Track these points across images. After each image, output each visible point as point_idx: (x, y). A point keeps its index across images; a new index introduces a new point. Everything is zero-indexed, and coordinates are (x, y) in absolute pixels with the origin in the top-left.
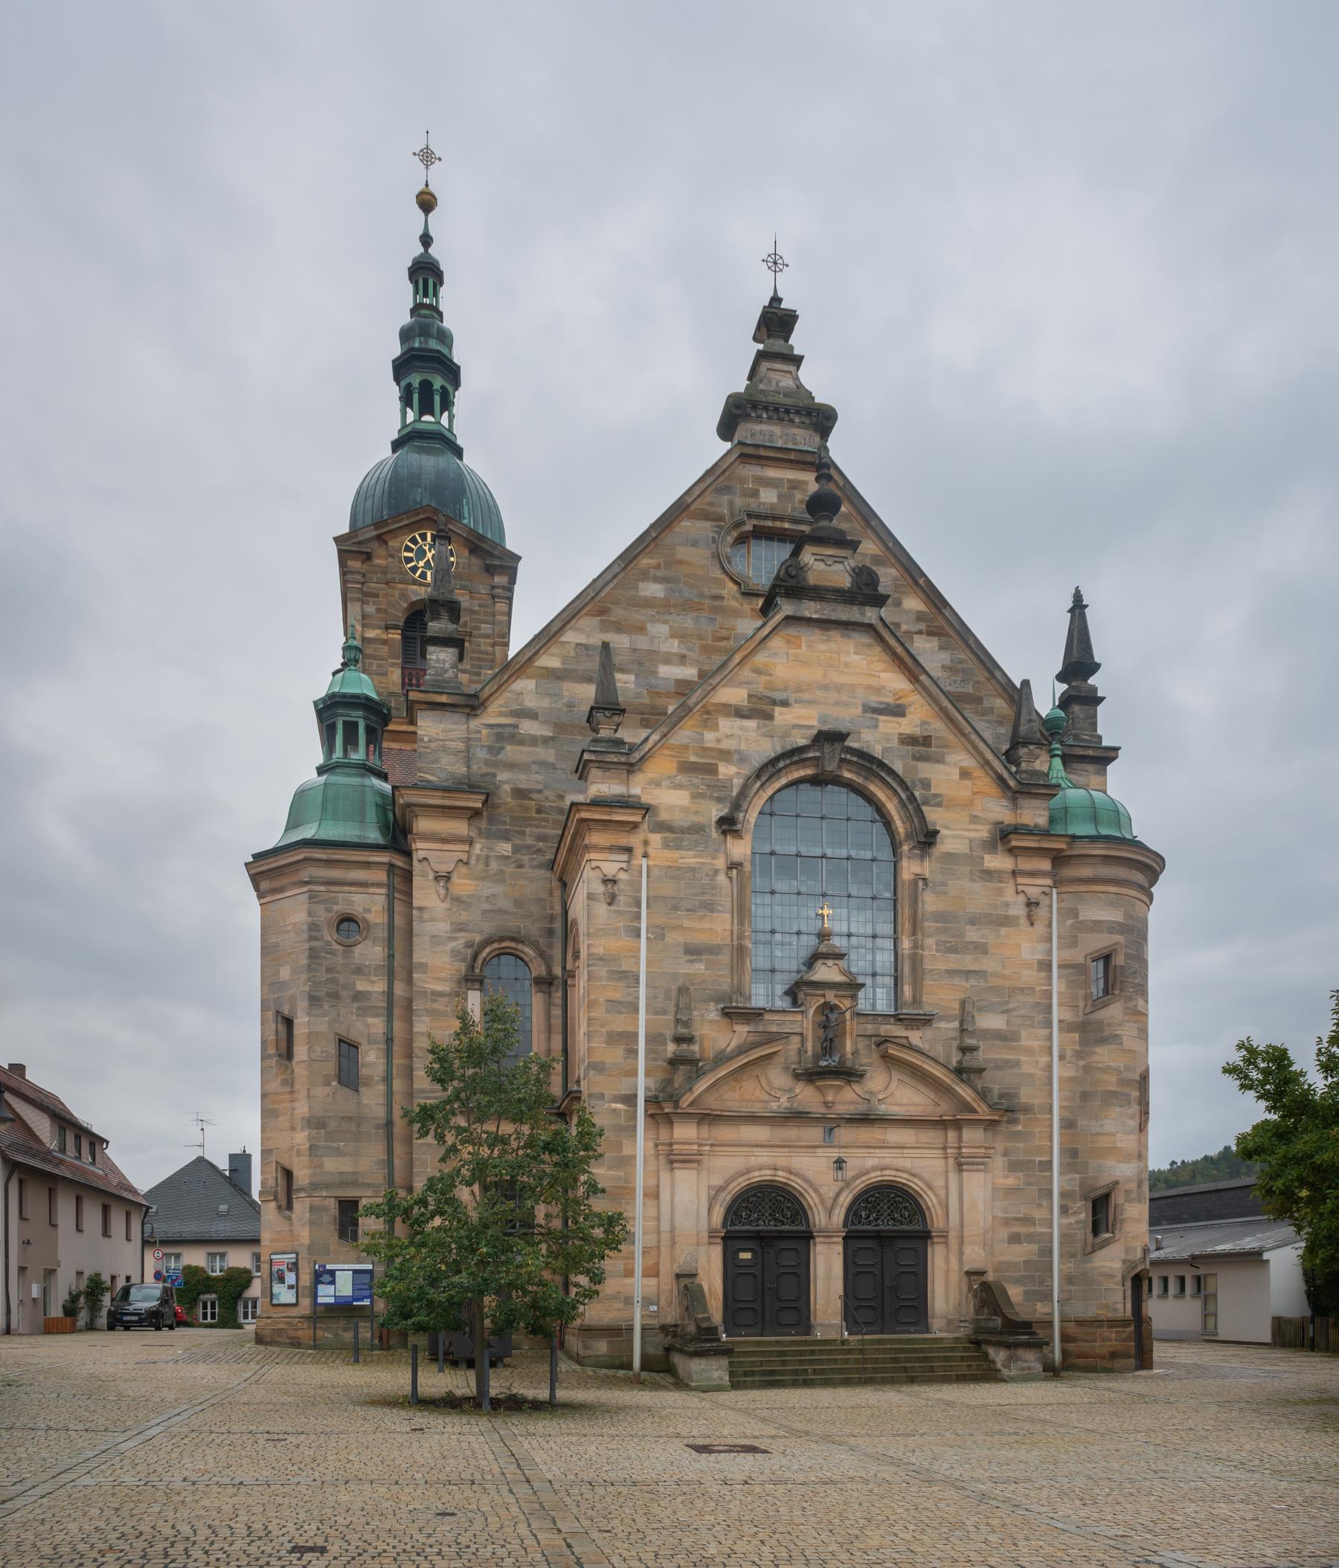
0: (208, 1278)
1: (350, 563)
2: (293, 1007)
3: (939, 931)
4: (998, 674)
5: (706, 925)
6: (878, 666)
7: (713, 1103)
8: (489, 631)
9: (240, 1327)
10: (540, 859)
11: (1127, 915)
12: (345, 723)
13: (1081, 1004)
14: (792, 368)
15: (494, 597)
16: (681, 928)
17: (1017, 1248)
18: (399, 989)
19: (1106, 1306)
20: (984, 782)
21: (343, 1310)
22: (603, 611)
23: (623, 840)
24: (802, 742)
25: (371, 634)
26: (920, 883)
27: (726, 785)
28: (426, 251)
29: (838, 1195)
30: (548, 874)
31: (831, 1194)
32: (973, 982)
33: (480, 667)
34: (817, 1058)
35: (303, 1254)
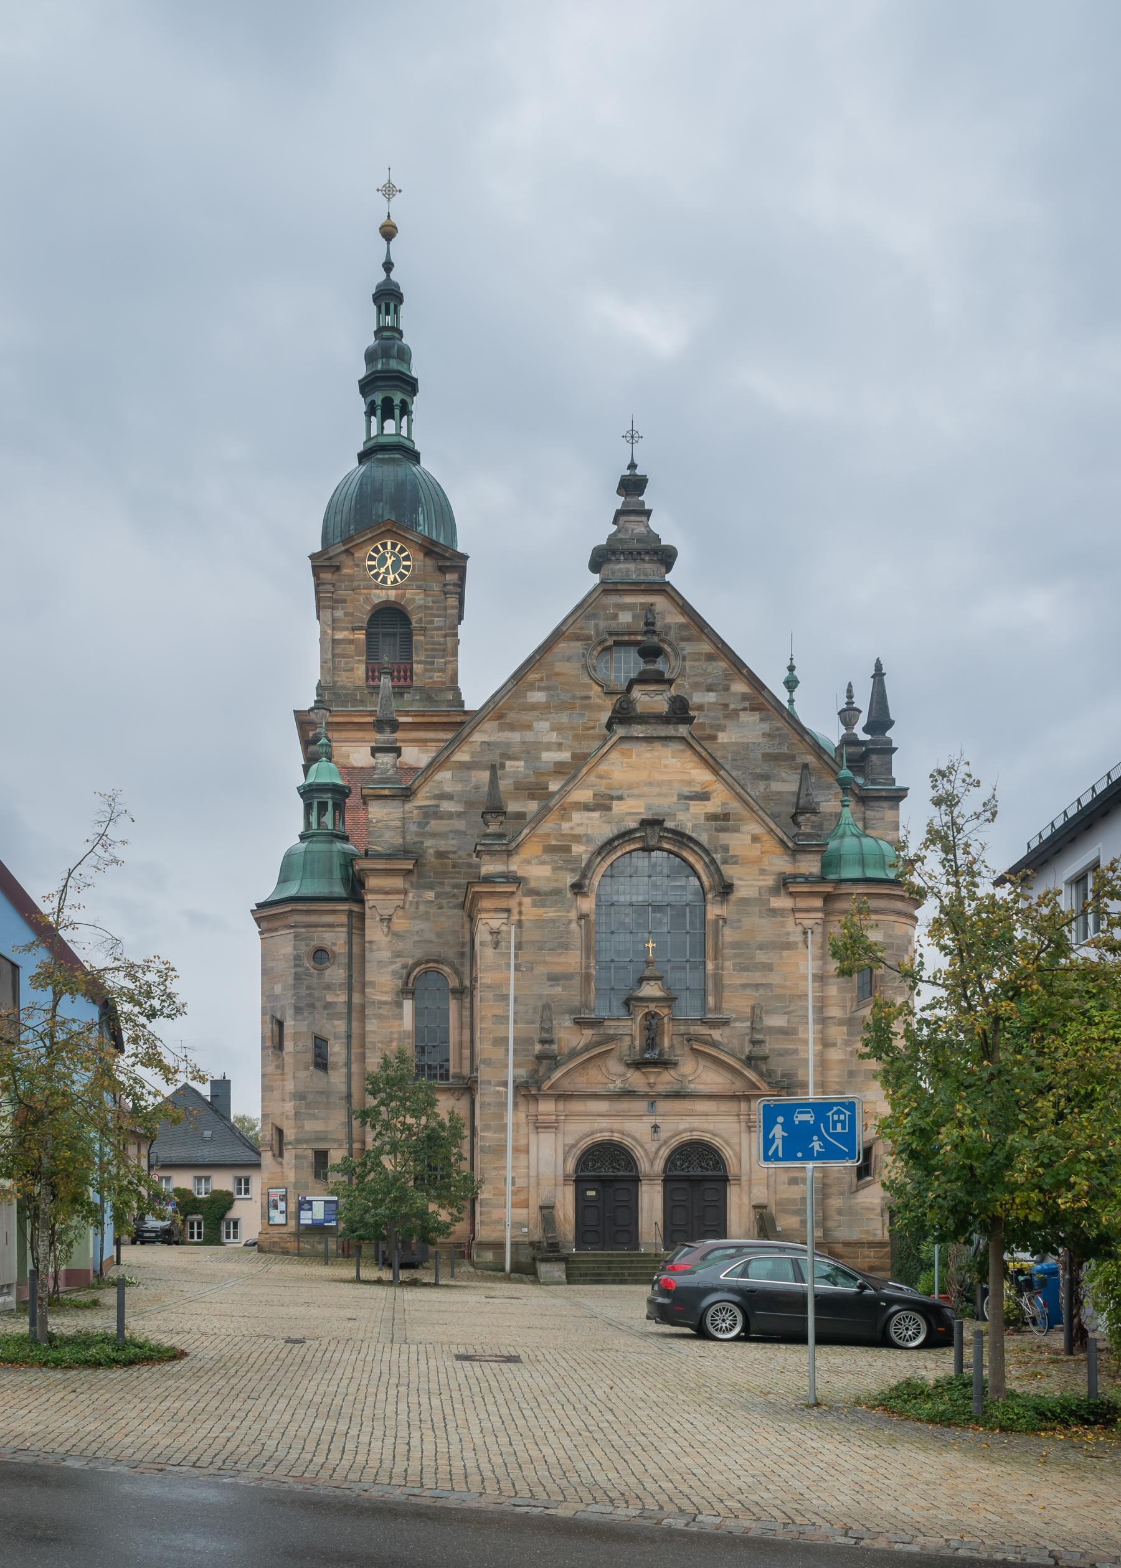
0: (195, 1199)
1: (322, 575)
2: (283, 1014)
3: (736, 956)
4: (807, 737)
5: (563, 959)
6: (690, 765)
7: (567, 1086)
8: (441, 624)
9: (223, 1244)
10: (455, 901)
11: (886, 935)
12: (319, 803)
13: (848, 1004)
14: (644, 519)
15: (445, 594)
16: (545, 963)
17: (795, 1188)
18: (356, 998)
19: (868, 1232)
20: (770, 844)
21: (317, 1229)
22: (500, 716)
23: (504, 904)
24: (633, 825)
25: (340, 635)
26: (721, 922)
27: (578, 859)
28: (388, 276)
29: (658, 1149)
30: (460, 912)
31: (653, 1149)
32: (761, 992)
33: (433, 657)
34: (643, 1051)
35: (290, 1189)
